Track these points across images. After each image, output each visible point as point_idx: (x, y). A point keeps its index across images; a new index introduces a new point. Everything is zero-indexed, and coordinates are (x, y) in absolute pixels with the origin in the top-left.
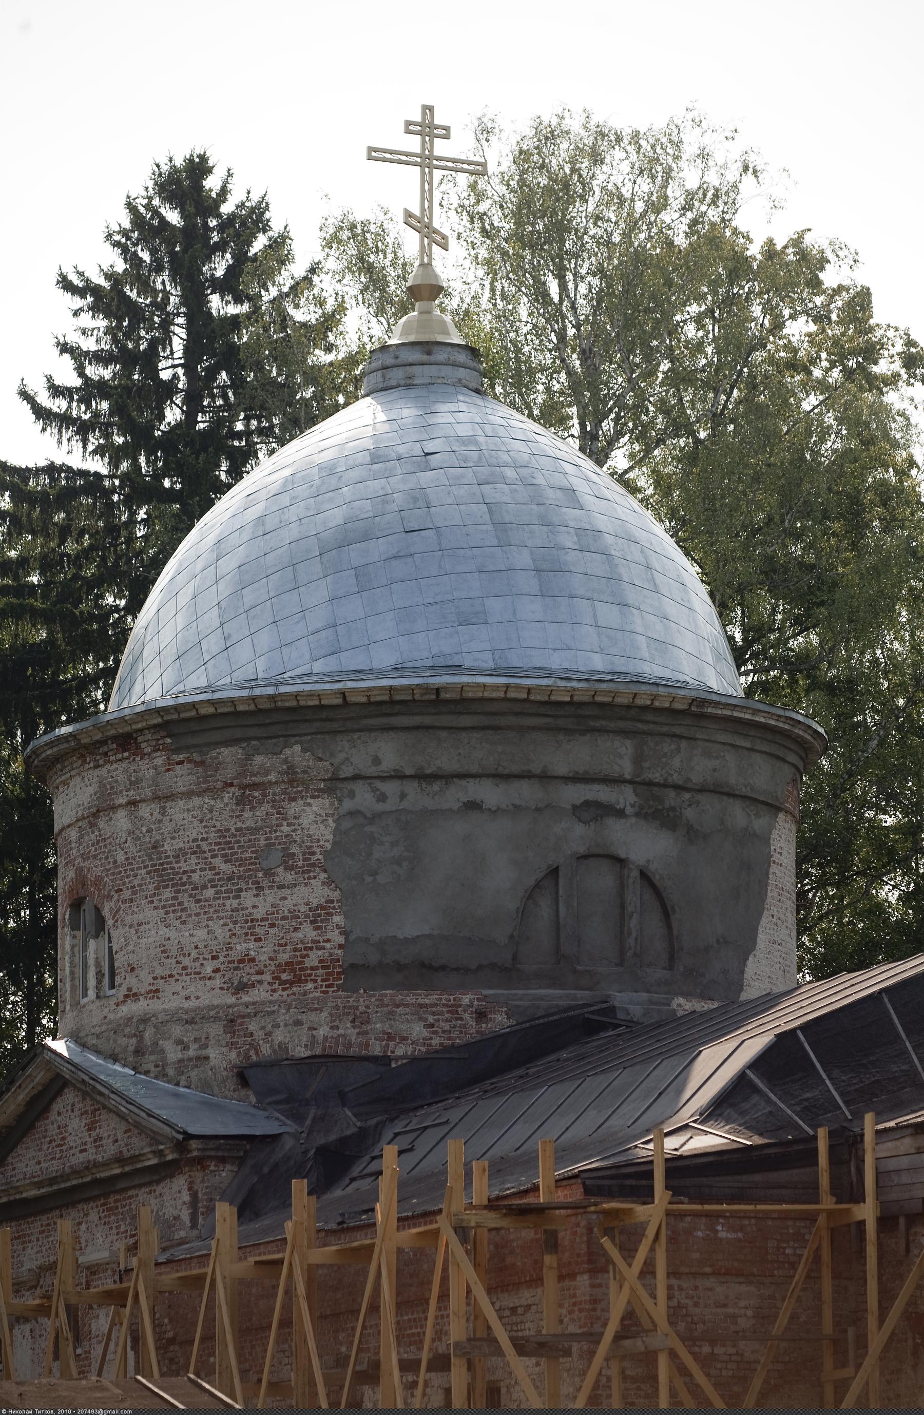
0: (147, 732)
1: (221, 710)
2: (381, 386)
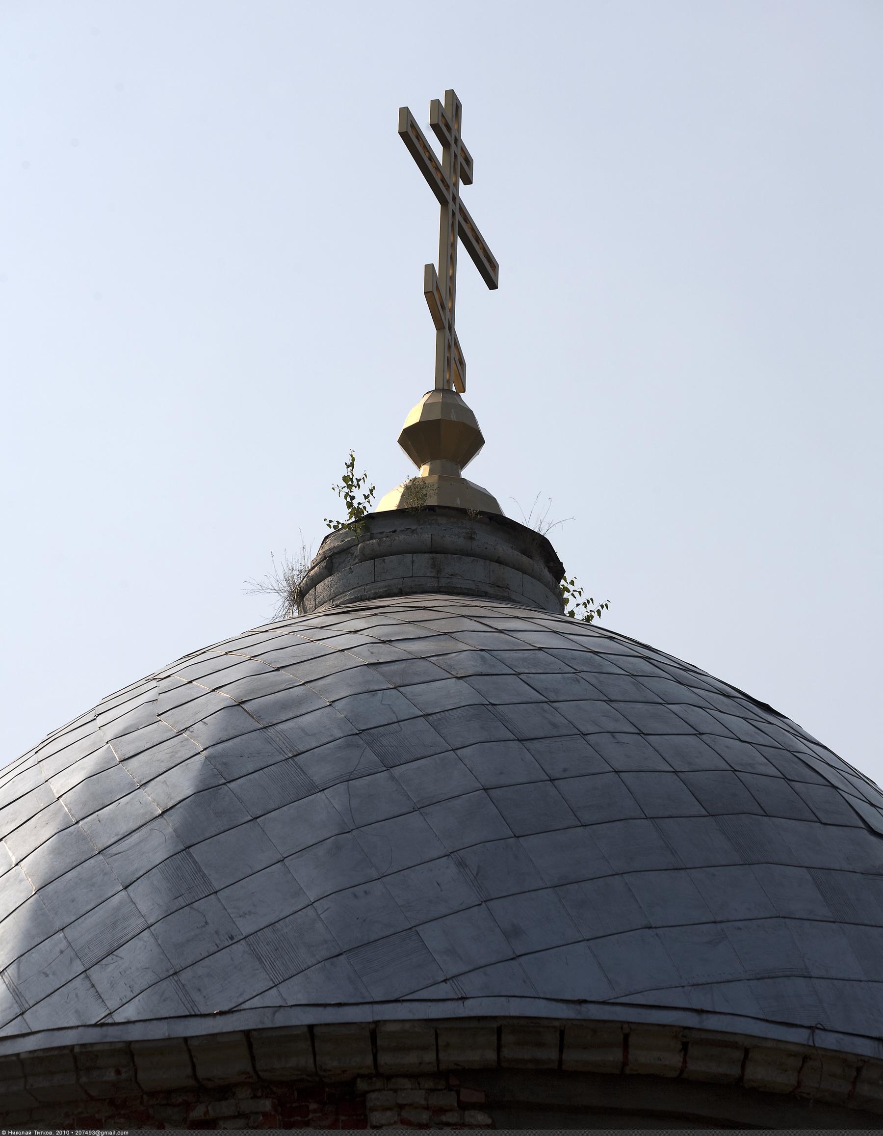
0: (407, 1083)
1: (699, 1067)
2: (434, 583)
